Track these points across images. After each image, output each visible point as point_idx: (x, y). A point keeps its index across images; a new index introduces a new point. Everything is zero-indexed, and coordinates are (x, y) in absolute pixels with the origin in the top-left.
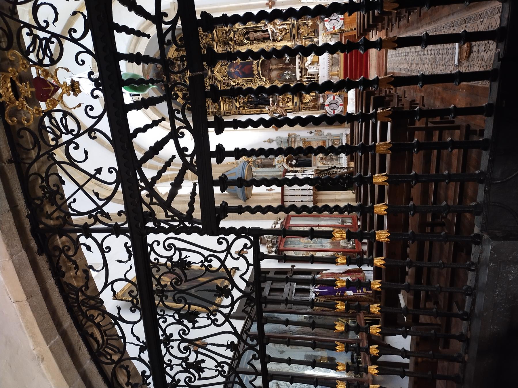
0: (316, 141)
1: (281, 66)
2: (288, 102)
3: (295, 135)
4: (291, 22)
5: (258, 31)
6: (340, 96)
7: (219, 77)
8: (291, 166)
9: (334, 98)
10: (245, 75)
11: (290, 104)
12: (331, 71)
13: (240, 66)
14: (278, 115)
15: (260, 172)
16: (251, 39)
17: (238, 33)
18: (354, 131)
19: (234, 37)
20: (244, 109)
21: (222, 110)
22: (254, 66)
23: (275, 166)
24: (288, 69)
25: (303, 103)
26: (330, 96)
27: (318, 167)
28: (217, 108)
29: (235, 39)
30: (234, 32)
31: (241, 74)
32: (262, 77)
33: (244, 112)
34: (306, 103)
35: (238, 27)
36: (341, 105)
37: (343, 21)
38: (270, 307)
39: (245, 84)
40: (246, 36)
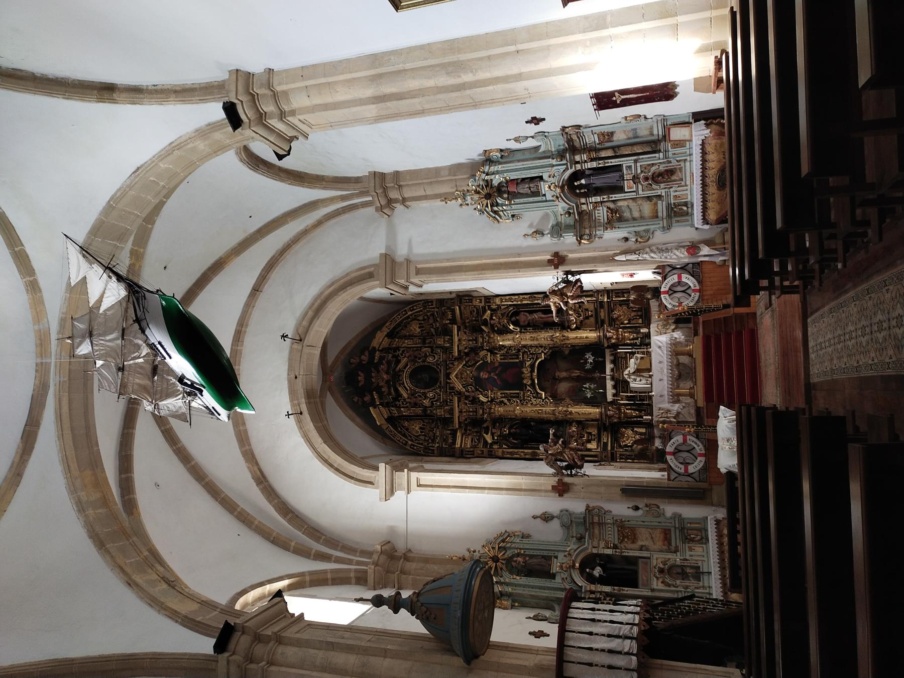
0: (647, 527)
1: (576, 373)
2: (589, 441)
3: (600, 508)
4: (598, 298)
5: (536, 312)
6: (697, 437)
7: (459, 386)
8: (591, 579)
9: (685, 440)
10: (506, 386)
11: (592, 446)
12: (678, 387)
13: (499, 369)
14: (565, 464)
15: (520, 585)
16: (522, 324)
17: (499, 312)
18: (739, 515)
19: (491, 318)
20: (501, 447)
21: (458, 445)
22: (524, 370)
23: (553, 576)
24: (591, 380)
25: (620, 447)
26: (676, 435)
27: (653, 590)
28: (450, 441)
29: (492, 322)
30: (492, 310)
31: (499, 383)
32: (539, 391)
33: (500, 453)
34: (626, 446)
35: (499, 303)
36: (701, 455)
37: (698, 294)
38: (625, 630)
39: (505, 401)
40: (513, 319)
